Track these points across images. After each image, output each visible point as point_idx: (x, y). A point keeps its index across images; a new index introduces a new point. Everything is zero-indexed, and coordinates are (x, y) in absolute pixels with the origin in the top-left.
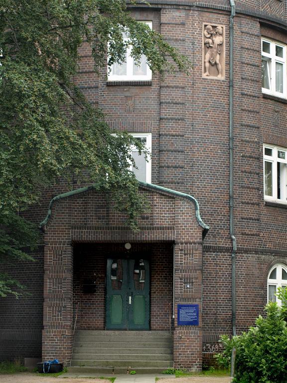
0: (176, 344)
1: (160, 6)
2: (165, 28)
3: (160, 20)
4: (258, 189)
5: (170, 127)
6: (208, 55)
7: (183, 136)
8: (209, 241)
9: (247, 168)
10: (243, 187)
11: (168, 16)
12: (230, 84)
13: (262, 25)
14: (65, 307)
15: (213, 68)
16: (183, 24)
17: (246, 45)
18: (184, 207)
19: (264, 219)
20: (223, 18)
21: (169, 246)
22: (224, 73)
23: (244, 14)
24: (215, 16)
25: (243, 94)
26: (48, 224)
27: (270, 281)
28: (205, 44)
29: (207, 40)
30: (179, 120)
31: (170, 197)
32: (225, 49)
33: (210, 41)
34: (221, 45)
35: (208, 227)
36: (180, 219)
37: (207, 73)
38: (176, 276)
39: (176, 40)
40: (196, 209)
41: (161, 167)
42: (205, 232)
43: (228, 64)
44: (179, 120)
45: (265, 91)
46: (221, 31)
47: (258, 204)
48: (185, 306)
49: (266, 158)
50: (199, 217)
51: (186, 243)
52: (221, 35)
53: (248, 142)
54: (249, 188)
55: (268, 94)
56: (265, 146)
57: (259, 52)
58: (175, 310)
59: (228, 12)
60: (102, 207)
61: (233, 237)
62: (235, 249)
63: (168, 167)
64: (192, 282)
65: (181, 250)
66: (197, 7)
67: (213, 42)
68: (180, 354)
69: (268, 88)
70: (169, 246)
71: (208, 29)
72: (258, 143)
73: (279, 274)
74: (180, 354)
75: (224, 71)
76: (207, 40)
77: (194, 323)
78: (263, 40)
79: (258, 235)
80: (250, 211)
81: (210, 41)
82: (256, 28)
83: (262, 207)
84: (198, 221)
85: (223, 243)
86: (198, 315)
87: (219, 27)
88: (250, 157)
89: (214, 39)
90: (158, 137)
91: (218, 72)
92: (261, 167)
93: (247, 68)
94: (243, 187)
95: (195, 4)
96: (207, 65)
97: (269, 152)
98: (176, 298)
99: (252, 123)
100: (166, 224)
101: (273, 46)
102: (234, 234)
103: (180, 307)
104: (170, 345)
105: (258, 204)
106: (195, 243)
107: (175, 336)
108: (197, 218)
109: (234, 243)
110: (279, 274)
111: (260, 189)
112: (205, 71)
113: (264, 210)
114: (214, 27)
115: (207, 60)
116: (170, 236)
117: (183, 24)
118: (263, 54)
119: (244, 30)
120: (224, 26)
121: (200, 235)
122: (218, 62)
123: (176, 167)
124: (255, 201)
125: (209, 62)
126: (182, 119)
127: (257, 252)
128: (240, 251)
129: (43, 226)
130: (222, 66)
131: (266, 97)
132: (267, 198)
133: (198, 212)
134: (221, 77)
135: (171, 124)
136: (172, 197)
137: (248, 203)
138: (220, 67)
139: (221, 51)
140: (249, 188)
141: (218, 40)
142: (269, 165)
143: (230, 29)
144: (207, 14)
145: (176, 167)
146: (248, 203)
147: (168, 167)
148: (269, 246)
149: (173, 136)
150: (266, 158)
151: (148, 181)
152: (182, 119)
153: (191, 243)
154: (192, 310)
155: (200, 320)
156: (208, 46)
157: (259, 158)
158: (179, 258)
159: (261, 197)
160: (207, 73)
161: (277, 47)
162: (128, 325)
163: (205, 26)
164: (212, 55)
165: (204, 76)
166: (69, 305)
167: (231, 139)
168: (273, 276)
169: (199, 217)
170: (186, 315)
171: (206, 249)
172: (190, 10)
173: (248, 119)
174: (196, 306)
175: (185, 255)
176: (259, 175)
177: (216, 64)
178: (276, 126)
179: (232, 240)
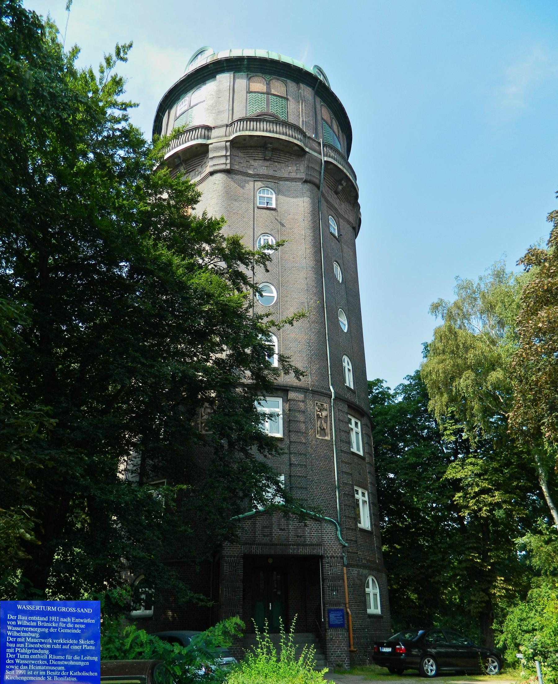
5: (298, 471)
6: (319, 423)
13: (349, 407)
15: (322, 432)
17: (341, 418)
18: (328, 528)
19: (360, 541)
21: (318, 559)
24: (322, 398)
27: (367, 589)
34: (326, 417)
36: (326, 538)
37: (319, 435)
39: (299, 411)
40: (337, 530)
48: (332, 610)
51: (331, 557)
52: (326, 410)
60: (266, 527)
64: (338, 590)
65: (328, 563)
67: (322, 415)
68: (332, 654)
70: (318, 559)
71: (318, 406)
74: (332, 654)
79: (357, 553)
82: (346, 409)
83: (358, 533)
84: (339, 540)
86: (343, 618)
87: (325, 405)
90: (289, 477)
96: (319, 429)
99: (348, 471)
100: (315, 541)
101: (353, 420)
108: (338, 537)
115: (318, 426)
116: (321, 552)
133: (339, 533)
135: (298, 468)
138: (326, 431)
141: (324, 413)
144: (317, 396)
149: (300, 477)
153: (334, 557)
154: (340, 614)
157: (354, 496)
164: (321, 423)
168: (368, 587)
169: (340, 536)
175: (331, 566)
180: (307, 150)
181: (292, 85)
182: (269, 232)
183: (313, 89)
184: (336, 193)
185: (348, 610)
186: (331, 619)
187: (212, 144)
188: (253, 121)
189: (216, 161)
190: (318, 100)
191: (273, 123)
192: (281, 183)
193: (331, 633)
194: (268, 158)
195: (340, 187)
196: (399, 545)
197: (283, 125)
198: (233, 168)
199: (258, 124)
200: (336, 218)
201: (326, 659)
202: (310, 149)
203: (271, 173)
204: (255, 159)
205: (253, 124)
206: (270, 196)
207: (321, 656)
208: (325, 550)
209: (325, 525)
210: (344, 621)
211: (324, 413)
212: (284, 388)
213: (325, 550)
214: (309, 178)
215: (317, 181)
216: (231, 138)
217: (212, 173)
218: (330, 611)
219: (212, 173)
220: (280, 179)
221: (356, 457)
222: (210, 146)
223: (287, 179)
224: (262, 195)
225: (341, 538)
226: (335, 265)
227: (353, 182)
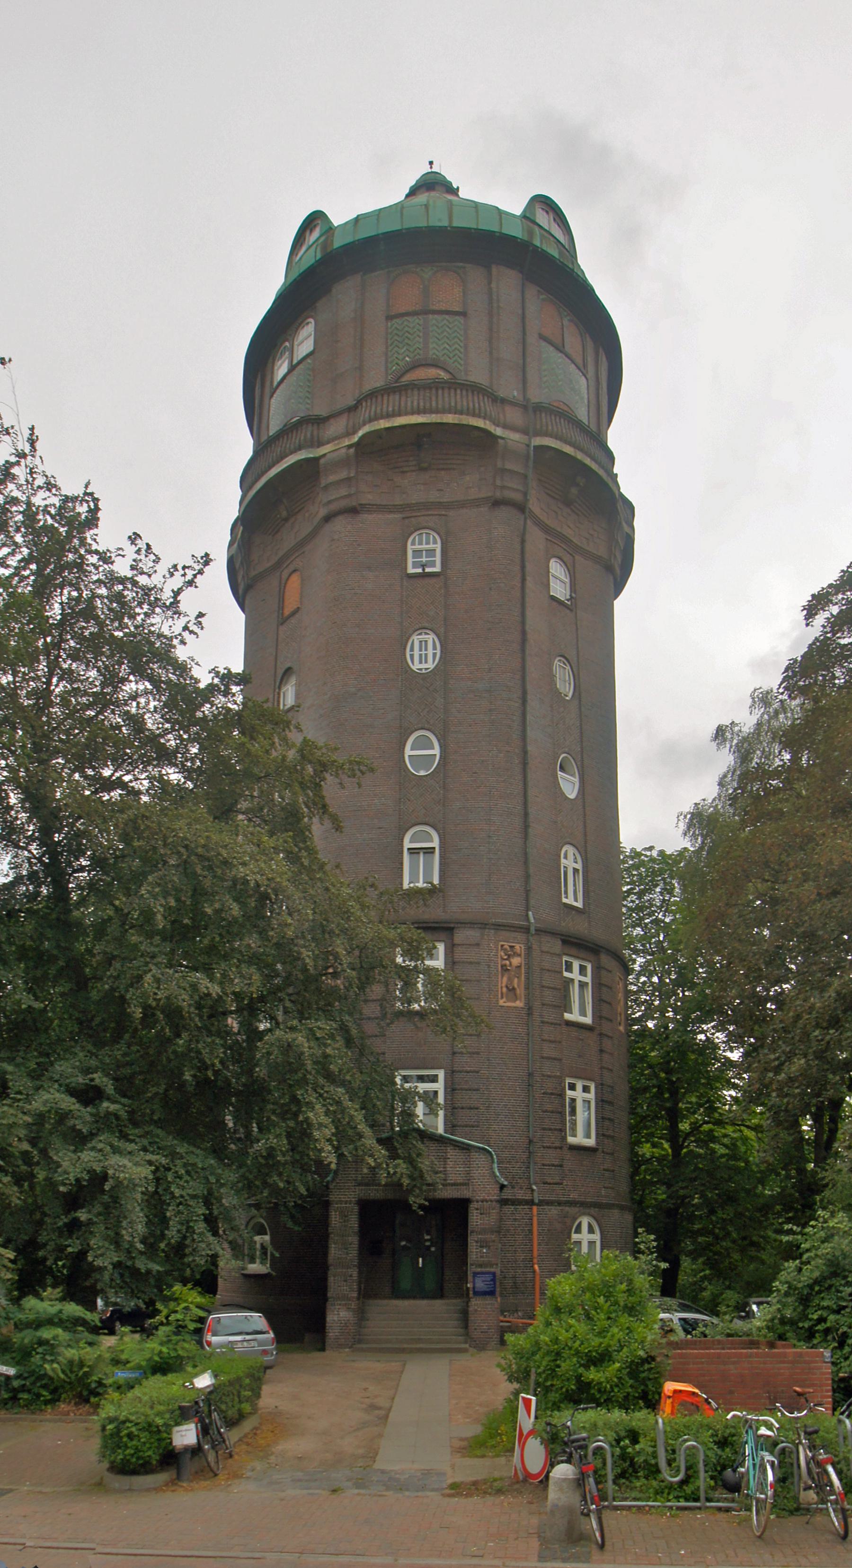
0: (472, 1317)
1: (452, 925)
2: (458, 950)
3: (453, 940)
4: (561, 1130)
6: (505, 979)
7: (478, 1072)
8: (507, 1194)
9: (548, 1107)
10: (544, 1129)
11: (460, 936)
12: (529, 1010)
14: (351, 1276)
16: (478, 945)
18: (479, 1160)
20: (520, 936)
21: (461, 1206)
22: (523, 999)
23: (545, 932)
25: (543, 1022)
26: (333, 1179)
27: (575, 1237)
28: (502, 966)
29: (504, 962)
30: (474, 1053)
31: (464, 1149)
32: (523, 971)
33: (507, 962)
34: (519, 967)
35: (506, 1183)
38: (472, 1241)
40: (493, 1162)
41: (454, 1108)
42: (502, 1187)
43: (527, 988)
44: (474, 1053)
45: (567, 1016)
46: (519, 952)
47: (561, 1148)
48: (479, 1273)
49: (570, 1093)
50: (496, 1171)
51: (482, 1201)
52: (519, 955)
53: (549, 1076)
54: (550, 1129)
55: (270, 305)
56: (568, 1080)
57: (561, 973)
58: (470, 1278)
59: (527, 930)
61: (534, 1187)
62: (536, 1201)
63: (462, 1108)
64: (489, 1247)
65: (477, 1209)
66: (493, 925)
67: (511, 964)
69: (571, 1013)
70: (461, 1206)
71: (506, 949)
72: (560, 1077)
73: (585, 1228)
75: (523, 996)
76: (504, 962)
77: (492, 1293)
78: (565, 958)
80: (552, 1157)
81: (507, 962)
84: (495, 1176)
85: (521, 1195)
86: (495, 1284)
87: (517, 947)
88: (552, 1094)
89: (512, 960)
91: (516, 998)
92: (564, 1106)
93: (547, 992)
94: (544, 1129)
95: (490, 921)
96: (505, 990)
97: (572, 1087)
98: (472, 1265)
99: (554, 1054)
100: (460, 1180)
102: (535, 1184)
103: (475, 1274)
104: (465, 1316)
105: (561, 1148)
106: (491, 1201)
107: (471, 1309)
108: (494, 1172)
109: (536, 1194)
110: (585, 1228)
111: (562, 1130)
112: (502, 998)
113: (568, 1155)
114: (512, 947)
115: (504, 985)
116: (464, 1193)
117: (478, 945)
118: (566, 974)
119: (545, 949)
120: (522, 946)
121: (497, 1191)
122: (516, 986)
123: (471, 1108)
124: (557, 1144)
125: (507, 987)
126: (478, 1053)
127: (560, 1203)
128: (541, 1203)
129: (328, 1182)
130: (521, 991)
131: (569, 1024)
132: (571, 1140)
133: (495, 1165)
134: (519, 1004)
136: (466, 1148)
137: (549, 1147)
138: (518, 992)
139: (520, 974)
140: (550, 1129)
141: (516, 961)
142: (573, 1100)
143: (529, 949)
144: (504, 933)
145: (471, 1108)
146: (549, 1147)
147: (462, 1108)
148: (574, 1196)
150: (570, 1093)
151: (441, 1130)
152: (478, 1053)
153: (487, 1201)
155: (498, 1290)
156: (505, 969)
157: (562, 1095)
158: (475, 1219)
159: (564, 1138)
160: (504, 999)
161: (581, 966)
162: (419, 1292)
163: (502, 946)
165: (501, 1002)
166: (355, 1273)
167: (530, 1075)
168: (578, 1230)
169: (496, 1171)
170: (481, 1284)
171: (504, 1202)
172: (485, 928)
173: (548, 1050)
174: (494, 1274)
176: (562, 1114)
177: (514, 989)
178: (580, 1056)
179: (533, 1190)
180: (499, 432)
181: (475, 275)
182: (427, 625)
183: (521, 272)
184: (568, 503)
185: (536, 1267)
186: (477, 1285)
187: (324, 455)
188: (394, 392)
189: (334, 494)
190: (532, 291)
191: (430, 388)
192: (451, 513)
193: (476, 1303)
194: (425, 465)
195: (574, 491)
196: (685, 1153)
197: (449, 388)
198: (363, 502)
199: (403, 398)
200: (567, 558)
201: (467, 1335)
202: (505, 426)
203: (433, 496)
204: (403, 472)
205: (392, 402)
206: (431, 546)
207: (462, 1331)
208: (473, 1191)
209: (475, 1155)
210: (495, 1287)
211: (516, 961)
212: (445, 925)
213: (473, 1191)
214: (498, 494)
215: (517, 497)
216: (356, 439)
217: (327, 519)
218: (475, 1274)
219: (327, 519)
220: (448, 506)
221: (575, 1029)
222: (322, 461)
223: (462, 505)
224: (417, 547)
225: (498, 1174)
226: (557, 663)
227: (601, 472)
